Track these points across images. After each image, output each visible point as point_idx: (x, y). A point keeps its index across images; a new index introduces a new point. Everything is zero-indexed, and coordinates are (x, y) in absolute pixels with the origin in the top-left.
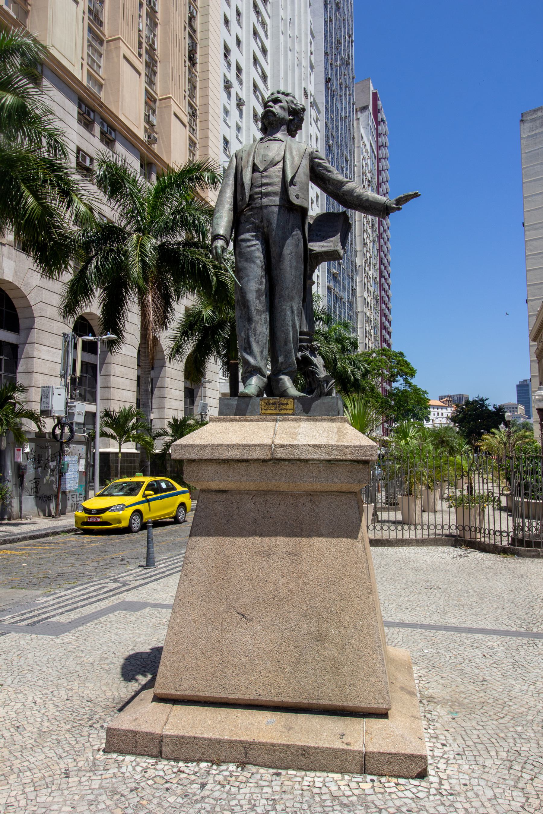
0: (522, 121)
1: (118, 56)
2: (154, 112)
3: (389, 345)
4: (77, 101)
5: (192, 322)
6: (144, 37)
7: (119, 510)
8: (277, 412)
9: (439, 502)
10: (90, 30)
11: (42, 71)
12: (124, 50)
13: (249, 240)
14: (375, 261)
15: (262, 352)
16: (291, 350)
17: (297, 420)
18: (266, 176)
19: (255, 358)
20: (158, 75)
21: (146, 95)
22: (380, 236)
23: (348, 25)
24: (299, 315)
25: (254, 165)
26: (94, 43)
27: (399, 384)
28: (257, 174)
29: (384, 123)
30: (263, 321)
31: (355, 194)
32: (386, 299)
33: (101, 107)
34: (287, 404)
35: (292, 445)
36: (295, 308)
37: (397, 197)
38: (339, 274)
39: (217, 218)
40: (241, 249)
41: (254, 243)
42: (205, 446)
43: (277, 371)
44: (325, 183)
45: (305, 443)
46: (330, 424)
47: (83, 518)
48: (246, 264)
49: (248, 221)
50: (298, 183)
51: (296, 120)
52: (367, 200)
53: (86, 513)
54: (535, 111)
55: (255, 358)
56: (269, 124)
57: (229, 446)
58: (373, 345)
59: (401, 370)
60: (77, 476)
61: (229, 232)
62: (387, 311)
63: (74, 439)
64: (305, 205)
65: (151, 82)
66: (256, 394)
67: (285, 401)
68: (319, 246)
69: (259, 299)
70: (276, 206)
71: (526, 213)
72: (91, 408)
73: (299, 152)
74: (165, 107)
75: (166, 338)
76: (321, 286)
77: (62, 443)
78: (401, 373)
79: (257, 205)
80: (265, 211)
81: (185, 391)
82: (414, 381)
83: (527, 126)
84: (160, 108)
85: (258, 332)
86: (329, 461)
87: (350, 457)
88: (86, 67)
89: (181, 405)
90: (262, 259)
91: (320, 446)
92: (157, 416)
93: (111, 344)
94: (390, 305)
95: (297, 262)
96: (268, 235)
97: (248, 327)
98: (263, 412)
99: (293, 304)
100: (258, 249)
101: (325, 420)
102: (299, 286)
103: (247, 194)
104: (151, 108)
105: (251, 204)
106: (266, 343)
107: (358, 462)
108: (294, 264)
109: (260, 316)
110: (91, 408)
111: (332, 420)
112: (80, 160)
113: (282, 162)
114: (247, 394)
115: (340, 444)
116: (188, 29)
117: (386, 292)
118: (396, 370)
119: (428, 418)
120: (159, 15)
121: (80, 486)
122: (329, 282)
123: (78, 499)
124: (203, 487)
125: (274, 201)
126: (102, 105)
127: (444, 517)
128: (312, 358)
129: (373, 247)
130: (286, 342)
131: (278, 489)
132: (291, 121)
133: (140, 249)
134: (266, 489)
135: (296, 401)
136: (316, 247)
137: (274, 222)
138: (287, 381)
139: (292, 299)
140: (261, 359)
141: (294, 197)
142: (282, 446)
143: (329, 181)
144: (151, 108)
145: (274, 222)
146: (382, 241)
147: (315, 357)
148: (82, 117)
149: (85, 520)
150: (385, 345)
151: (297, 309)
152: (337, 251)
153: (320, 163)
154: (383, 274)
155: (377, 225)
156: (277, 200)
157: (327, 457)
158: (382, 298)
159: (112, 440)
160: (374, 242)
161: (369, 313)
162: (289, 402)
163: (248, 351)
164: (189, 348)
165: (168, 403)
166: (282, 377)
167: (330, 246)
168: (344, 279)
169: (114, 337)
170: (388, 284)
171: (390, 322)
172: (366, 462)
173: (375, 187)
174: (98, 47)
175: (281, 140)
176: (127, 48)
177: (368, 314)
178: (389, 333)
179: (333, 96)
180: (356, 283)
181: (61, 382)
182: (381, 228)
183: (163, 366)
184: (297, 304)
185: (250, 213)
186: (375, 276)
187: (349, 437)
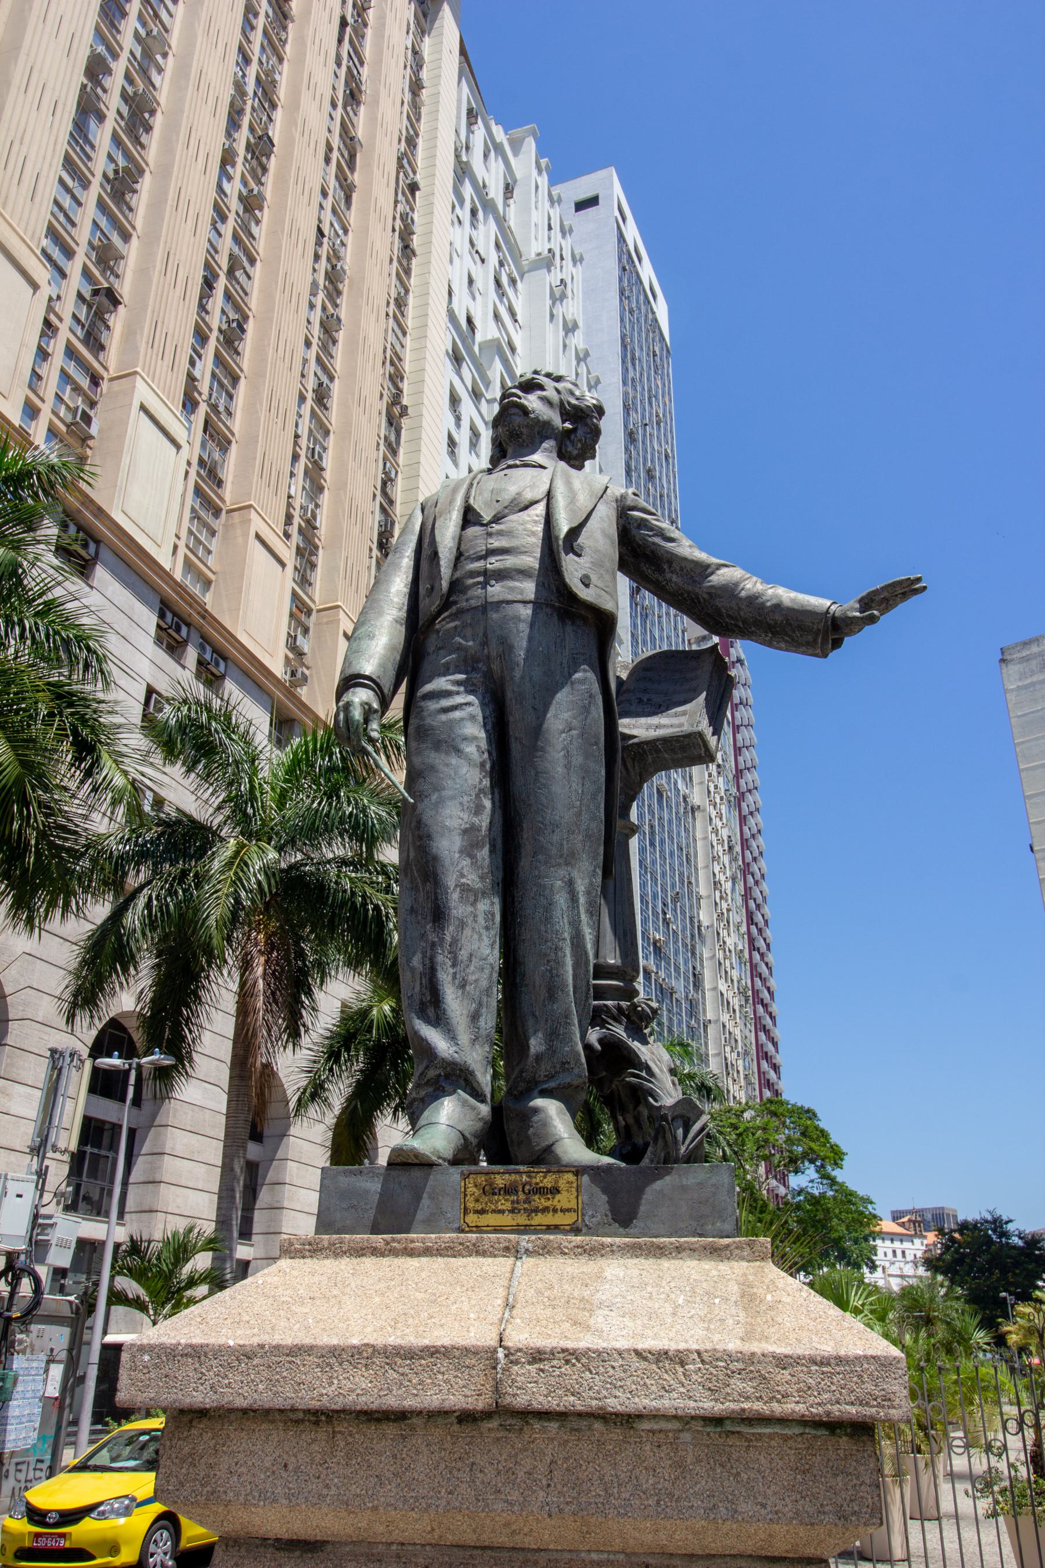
0: (1002, 661)
1: (246, 535)
2: (306, 631)
3: (777, 1093)
4: (158, 606)
5: (352, 1030)
6: (297, 507)
7: (119, 1514)
8: (521, 1219)
9: (945, 1487)
10: (198, 491)
11: (97, 553)
12: (256, 524)
13: (448, 694)
14: (738, 917)
15: (475, 1017)
16: (567, 1016)
17: (591, 1252)
18: (500, 533)
19: (451, 1034)
20: (319, 569)
21: (293, 601)
22: (746, 870)
23: (670, 503)
24: (593, 911)
26: (202, 514)
27: (805, 1180)
28: (473, 531)
29: (742, 664)
30: (481, 920)
31: (743, 594)
32: (765, 995)
33: (204, 617)
34: (555, 1191)
35: (573, 1353)
36: (581, 887)
37: (864, 594)
38: (666, 943)
40: (422, 719)
41: (459, 699)
42: (245, 1354)
45: (622, 1344)
47: (22, 1535)
48: (434, 758)
49: (445, 646)
51: (580, 432)
53: (32, 1521)
54: (1026, 644)
55: (453, 1038)
56: (514, 435)
57: (336, 1353)
58: (743, 1093)
59: (811, 1149)
60: (38, 1410)
62: (768, 1021)
63: (40, 1311)
64: (608, 605)
65: (304, 581)
66: (449, 1154)
67: (548, 1182)
68: (648, 727)
69: (472, 856)
70: (524, 602)
71: (1033, 828)
72: (93, 1229)
74: (327, 623)
75: (291, 1066)
77: (9, 1320)
78: (810, 1156)
79: (473, 603)
80: (495, 616)
82: (838, 1174)
83: (1013, 670)
84: (318, 624)
85: (463, 955)
86: (717, 1420)
87: (801, 1408)
88: (182, 551)
90: (484, 745)
91: (680, 1358)
93: (164, 1076)
94: (774, 1008)
95: (587, 756)
96: (502, 678)
97: (432, 937)
98: (472, 1219)
99: (575, 874)
100: (472, 718)
102: (593, 825)
104: (300, 623)
105: (455, 603)
106: (488, 992)
107: (833, 1426)
108: (578, 760)
109: (474, 904)
110: (93, 1229)
111: (715, 1252)
112: (151, 710)
114: (417, 1155)
115: (756, 1347)
116: (379, 498)
117: (764, 981)
118: (800, 1149)
119: (873, 1262)
120: (327, 475)
121: (41, 1437)
123: (31, 1476)
124: (228, 1527)
125: (521, 591)
126: (205, 614)
127: (964, 1535)
128: (635, 1045)
129: (733, 890)
130: (553, 989)
131: (519, 1541)
132: (568, 433)
133: (241, 868)
134: (470, 1538)
135: (585, 1179)
136: (638, 728)
138: (556, 1119)
139: (570, 859)
140: (474, 1041)
142: (537, 1356)
143: (670, 563)
144: (300, 623)
146: (750, 878)
147: (644, 1042)
148: (163, 634)
149: (27, 1544)
150: (767, 1094)
151: (588, 893)
152: (700, 735)
154: (757, 944)
155: (738, 848)
156: (529, 588)
157: (709, 1406)
158: (756, 992)
159: (137, 1314)
160: (734, 879)
161: (732, 1023)
162: (562, 1184)
163: (431, 1012)
164: (339, 1093)
166: (539, 1102)
167: (681, 725)
168: (676, 953)
169: (168, 1061)
170: (767, 964)
171: (775, 1044)
172: (862, 1430)
173: (731, 777)
174: (209, 519)
176: (266, 520)
177: (730, 1025)
178: (776, 1068)
179: (645, 617)
180: (702, 960)
181: (30, 1166)
182: (748, 853)
184: (585, 876)
185: (452, 625)
186: (740, 947)
187: (787, 1320)
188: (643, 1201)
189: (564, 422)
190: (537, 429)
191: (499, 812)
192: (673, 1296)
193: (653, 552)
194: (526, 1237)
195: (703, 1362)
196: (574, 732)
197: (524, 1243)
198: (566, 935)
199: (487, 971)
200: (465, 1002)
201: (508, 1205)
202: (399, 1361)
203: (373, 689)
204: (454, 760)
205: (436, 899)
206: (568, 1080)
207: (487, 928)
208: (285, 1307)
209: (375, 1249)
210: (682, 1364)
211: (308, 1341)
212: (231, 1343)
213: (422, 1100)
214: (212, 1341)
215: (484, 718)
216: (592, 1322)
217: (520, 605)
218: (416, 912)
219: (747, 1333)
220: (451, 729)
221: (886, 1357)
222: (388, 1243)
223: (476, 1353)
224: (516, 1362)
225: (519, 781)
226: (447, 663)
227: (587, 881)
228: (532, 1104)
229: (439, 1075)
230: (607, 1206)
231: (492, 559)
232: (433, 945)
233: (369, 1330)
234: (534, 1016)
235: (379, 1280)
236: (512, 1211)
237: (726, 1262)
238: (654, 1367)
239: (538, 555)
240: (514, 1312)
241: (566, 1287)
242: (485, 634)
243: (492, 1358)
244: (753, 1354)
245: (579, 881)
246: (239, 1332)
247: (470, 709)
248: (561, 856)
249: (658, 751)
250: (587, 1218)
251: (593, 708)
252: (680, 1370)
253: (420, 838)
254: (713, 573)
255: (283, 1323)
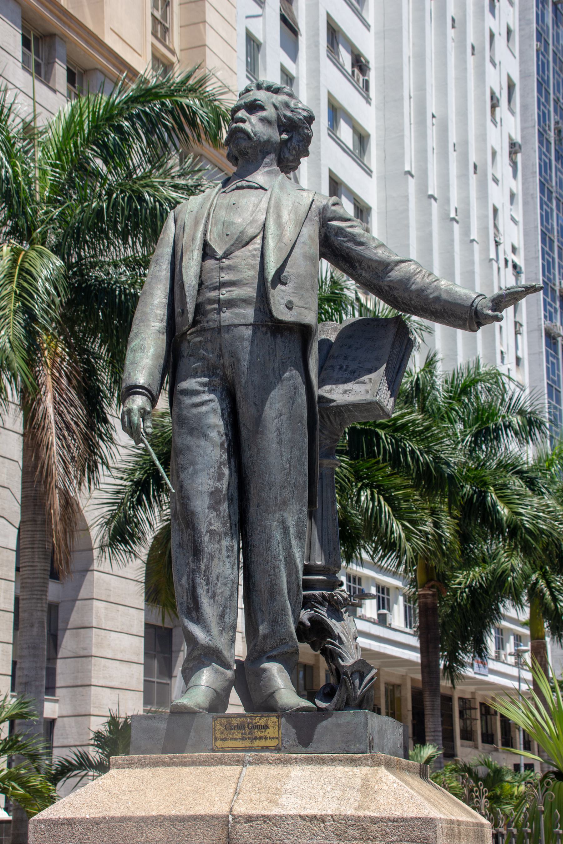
8: (247, 744)
13: (196, 393)
19: (207, 629)
24: (300, 536)
25: (206, 245)
28: (210, 263)
30: (224, 552)
31: (414, 287)
34: (266, 727)
35: (268, 817)
36: (291, 522)
39: (134, 350)
40: (181, 409)
41: (206, 397)
42: (96, 822)
43: (258, 652)
44: (353, 266)
45: (293, 812)
46: (348, 770)
48: (189, 441)
50: (292, 278)
52: (438, 299)
57: (143, 819)
61: (158, 376)
66: (206, 705)
67: (262, 722)
68: (345, 392)
69: (216, 510)
70: (246, 325)
73: (296, 213)
76: (524, 330)
80: (226, 336)
81: (147, 637)
85: (213, 577)
89: (135, 675)
91: (322, 819)
92: (67, 710)
96: (233, 380)
97: (193, 566)
98: (219, 744)
101: (341, 761)
103: (191, 307)
105: (200, 322)
108: (287, 436)
109: (219, 542)
111: (353, 762)
113: (260, 237)
115: (361, 813)
122: (550, 317)
125: (244, 316)
132: (284, 143)
135: (283, 720)
137: (245, 357)
140: (221, 632)
141: (283, 308)
142: (249, 819)
145: (245, 357)
147: (340, 619)
153: (340, 229)
156: (248, 313)
162: (270, 723)
163: (194, 614)
165: (101, 672)
166: (266, 665)
167: (366, 393)
175: (262, 188)
183: (86, 569)
185: (198, 339)
188: (316, 733)
189: (281, 134)
190: (259, 149)
191: (235, 475)
192: (325, 786)
193: (347, 254)
194: (249, 754)
195: (334, 821)
196: (284, 416)
197: (248, 758)
198: (282, 557)
199: (229, 585)
200: (216, 607)
201: (240, 736)
202: (178, 823)
203: (146, 395)
204: (203, 443)
205: (194, 540)
206: (285, 650)
207: (228, 557)
208: (116, 796)
209: (164, 762)
210: (324, 822)
211: (129, 814)
212: (88, 816)
213: (191, 669)
214: (77, 816)
215: (222, 410)
216: (279, 801)
217: (244, 328)
218: (183, 547)
219: (359, 806)
220: (200, 419)
221: (426, 818)
222: (171, 759)
223: (217, 818)
224: (238, 822)
225: (247, 455)
226: (196, 368)
227: (296, 517)
228: (262, 666)
229: (201, 654)
230: (295, 736)
231: (223, 291)
232: (194, 571)
233: (161, 807)
234: (262, 610)
235: (167, 780)
236: (242, 739)
237: (358, 767)
238: (309, 823)
239: (256, 286)
240: (239, 796)
241: (269, 782)
242: (220, 349)
243: (226, 820)
244: (359, 817)
245: (290, 519)
246: (92, 811)
247: (212, 404)
248: (276, 505)
249: (350, 411)
250: (284, 742)
251: (297, 396)
252: (322, 825)
253: (183, 498)
254: (392, 269)
255: (115, 805)
